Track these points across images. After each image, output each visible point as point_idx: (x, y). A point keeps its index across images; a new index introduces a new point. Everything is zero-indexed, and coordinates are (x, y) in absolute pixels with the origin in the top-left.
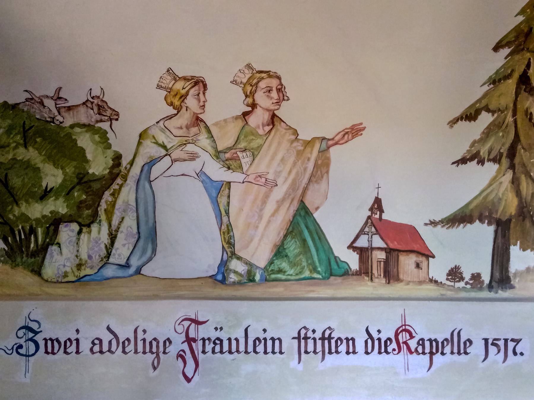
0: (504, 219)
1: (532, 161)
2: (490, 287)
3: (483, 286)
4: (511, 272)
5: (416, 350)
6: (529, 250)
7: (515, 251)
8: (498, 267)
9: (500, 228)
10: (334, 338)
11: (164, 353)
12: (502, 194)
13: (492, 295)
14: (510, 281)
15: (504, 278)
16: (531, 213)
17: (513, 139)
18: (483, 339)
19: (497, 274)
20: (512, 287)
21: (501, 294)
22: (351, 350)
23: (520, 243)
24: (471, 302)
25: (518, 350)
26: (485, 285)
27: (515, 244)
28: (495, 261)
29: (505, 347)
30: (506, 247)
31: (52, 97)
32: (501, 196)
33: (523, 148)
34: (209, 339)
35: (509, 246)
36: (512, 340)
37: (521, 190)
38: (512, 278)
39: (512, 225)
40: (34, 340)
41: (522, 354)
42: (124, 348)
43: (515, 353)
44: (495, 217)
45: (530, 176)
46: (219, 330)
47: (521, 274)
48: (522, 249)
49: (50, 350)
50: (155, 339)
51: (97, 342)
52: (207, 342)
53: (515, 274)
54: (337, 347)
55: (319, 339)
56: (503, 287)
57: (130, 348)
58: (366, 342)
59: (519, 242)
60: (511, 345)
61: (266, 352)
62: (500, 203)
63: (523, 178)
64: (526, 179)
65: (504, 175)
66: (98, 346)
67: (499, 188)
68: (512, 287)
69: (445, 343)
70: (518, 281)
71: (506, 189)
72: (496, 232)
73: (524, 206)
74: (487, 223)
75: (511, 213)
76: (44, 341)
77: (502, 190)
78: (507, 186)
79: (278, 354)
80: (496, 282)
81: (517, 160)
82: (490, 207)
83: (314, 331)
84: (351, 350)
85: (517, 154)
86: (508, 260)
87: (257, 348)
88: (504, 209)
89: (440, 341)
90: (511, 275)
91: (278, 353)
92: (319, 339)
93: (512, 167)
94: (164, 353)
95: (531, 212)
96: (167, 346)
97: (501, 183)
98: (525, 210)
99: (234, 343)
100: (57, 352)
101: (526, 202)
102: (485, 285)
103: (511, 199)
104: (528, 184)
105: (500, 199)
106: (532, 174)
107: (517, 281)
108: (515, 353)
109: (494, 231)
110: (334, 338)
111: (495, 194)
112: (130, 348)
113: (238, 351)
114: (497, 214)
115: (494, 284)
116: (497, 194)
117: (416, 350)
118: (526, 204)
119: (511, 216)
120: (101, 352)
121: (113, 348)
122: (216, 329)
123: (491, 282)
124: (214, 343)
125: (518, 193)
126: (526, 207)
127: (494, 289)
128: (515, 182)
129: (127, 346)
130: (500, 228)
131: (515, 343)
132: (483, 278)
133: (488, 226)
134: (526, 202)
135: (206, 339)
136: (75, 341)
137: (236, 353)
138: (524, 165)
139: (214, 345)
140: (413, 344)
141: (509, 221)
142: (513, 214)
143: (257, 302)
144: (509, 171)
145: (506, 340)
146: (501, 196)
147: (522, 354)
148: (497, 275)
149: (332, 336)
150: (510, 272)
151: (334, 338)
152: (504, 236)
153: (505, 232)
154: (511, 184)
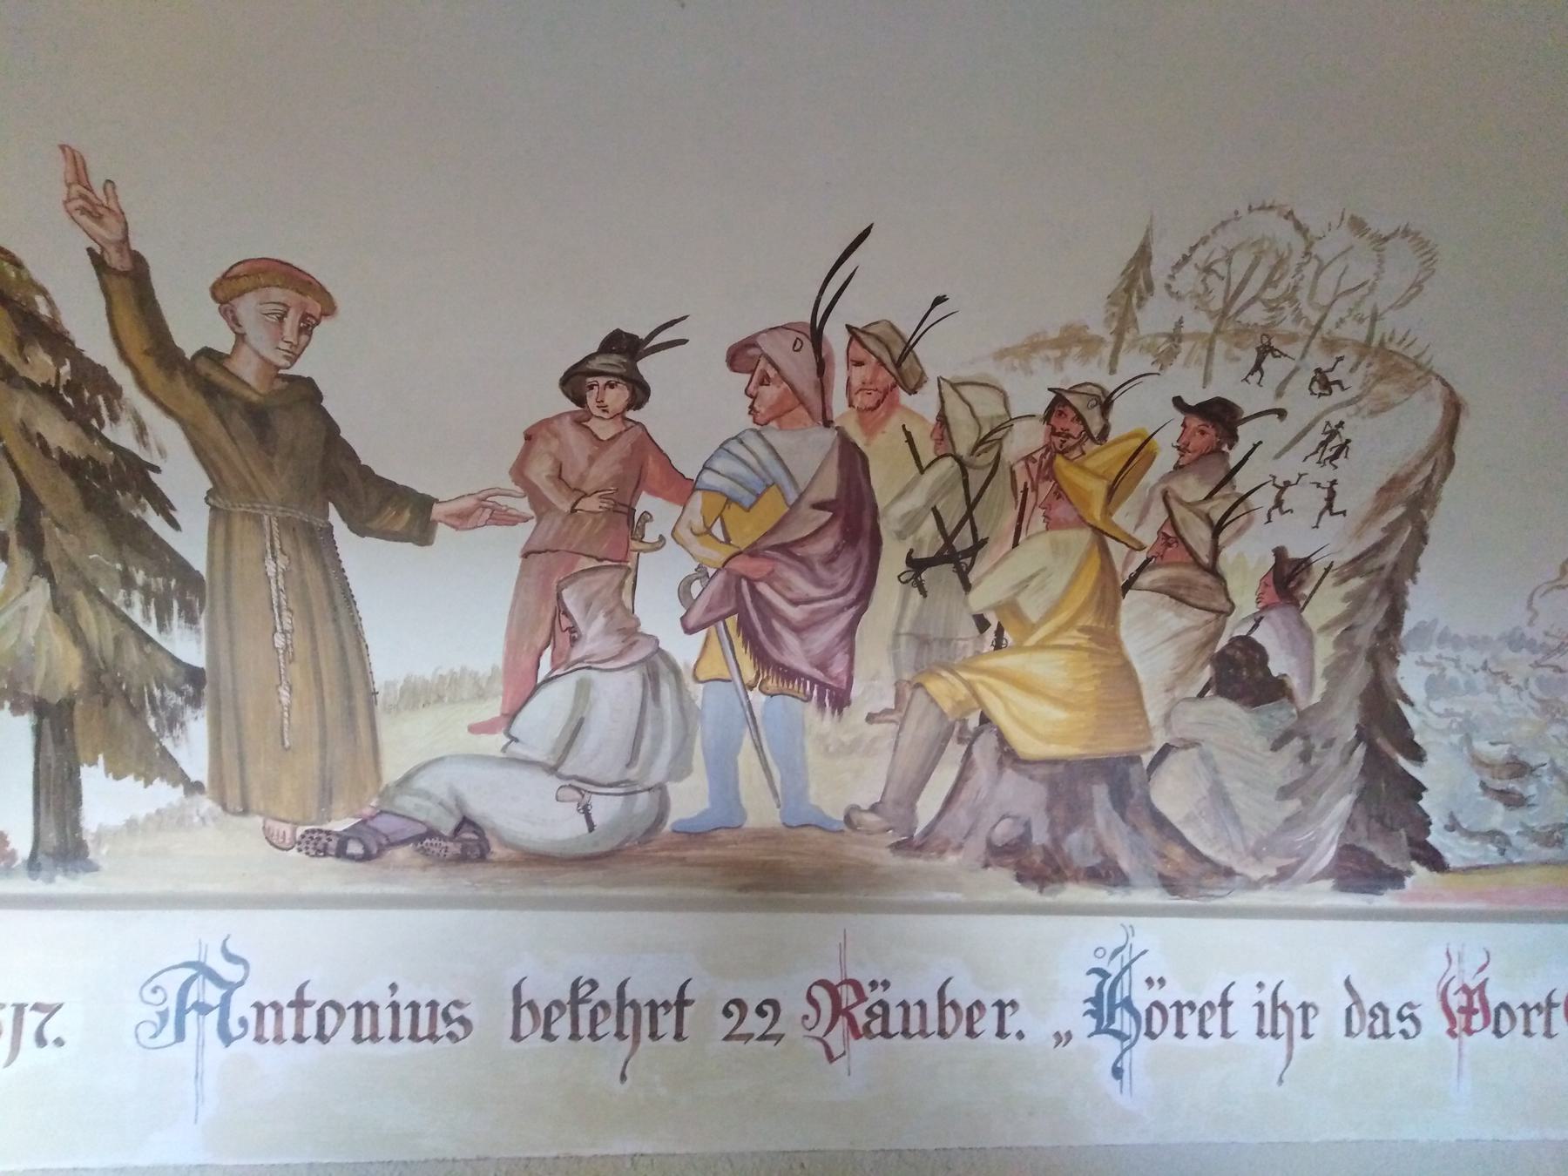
0: (54, 699)
1: (91, 557)
2: (33, 865)
3: (14, 866)
4: (87, 831)
5: (867, 1026)
6: (130, 779)
7: (93, 779)
8: (51, 817)
9: (46, 721)
10: (314, 1003)
11: (1306, 1035)
12: (34, 638)
13: (38, 887)
14: (87, 854)
15: (1358, 868)
16: (124, 687)
17: (20, 499)
18: (1255, 1005)
19: (51, 835)
20: (92, 868)
21: (65, 885)
22: (366, 1033)
23: (106, 758)
24: (1428, 924)
25: (50, 1033)
26: (19, 862)
27: (93, 763)
28: (42, 804)
29: (14, 1025)
30: (70, 769)
31: (652, 467)
32: (32, 642)
33: (59, 525)
34: (1191, 1005)
35: (78, 766)
36: (37, 1007)
37: (83, 626)
38: (90, 845)
39: (77, 713)
40: (43, 1011)
41: (59, 1042)
42: (548, 1024)
43: (41, 1040)
44: (30, 693)
45: (100, 595)
46: (1157, 985)
47: (115, 834)
48: (111, 775)
49: (1267, 1028)
50: (1380, 1005)
51: (733, 1008)
52: (1186, 1011)
53: (99, 837)
54: (594, 1023)
55: (291, 1005)
56: (69, 867)
57: (562, 1026)
58: (1349, 1011)
59: (101, 757)
60: (32, 1020)
61: (575, 1036)
62: (33, 659)
63: (80, 598)
64: (91, 601)
65: (27, 589)
66: (880, 1019)
67: (23, 620)
68: (92, 868)
69: (555, 1012)
70: (108, 853)
71: (42, 626)
72: (38, 731)
73: (100, 669)
74: (10, 708)
75: (70, 686)
76: (1256, 1008)
77: (31, 630)
78: (44, 616)
79: (313, 1043)
80: (47, 854)
81: (51, 554)
82: (9, 669)
83: (594, 985)
84: (366, 1033)
85: (47, 538)
86: (77, 800)
87: (598, 1028)
88: (46, 675)
89: (964, 1006)
90: (88, 838)
91: (270, 1042)
92: (291, 1005)
93: (43, 569)
94: (1306, 1035)
95: (121, 684)
96: (975, 1020)
97: (25, 609)
98: (105, 678)
99: (915, 1012)
100: (1161, 1033)
101: (102, 658)
102: (19, 862)
103: (61, 650)
104: (97, 614)
105: (32, 650)
106: (102, 590)
107: (104, 851)
108: (41, 1040)
109: (32, 728)
110: (313, 1003)
111: (16, 638)
112: (562, 1026)
113: (923, 1033)
114: (32, 687)
115: (41, 858)
116: (19, 637)
117: (867, 1026)
118: (104, 662)
119: (71, 693)
120: (885, 1034)
121: (1156, 1027)
122: (1149, 981)
123: (34, 855)
124: (1373, 1014)
125: (77, 636)
126: (107, 670)
127: (44, 873)
128: (60, 605)
129: (603, 1021)
130: (46, 721)
131: (44, 1016)
132: (11, 846)
133: (15, 715)
134: (102, 658)
135: (1006, 1002)
136: (353, 1010)
137: (899, 1036)
138: (73, 567)
139: (868, 1019)
140: (860, 1015)
141: (68, 705)
142: (76, 687)
143: (1080, 920)
144: (37, 581)
145: (20, 1009)
146: (32, 642)
147: (1020, 1035)
148: (51, 838)
149: (688, 996)
150: (84, 831)
151: (314, 1003)
152: (60, 741)
153: (62, 731)
154: (53, 613)
